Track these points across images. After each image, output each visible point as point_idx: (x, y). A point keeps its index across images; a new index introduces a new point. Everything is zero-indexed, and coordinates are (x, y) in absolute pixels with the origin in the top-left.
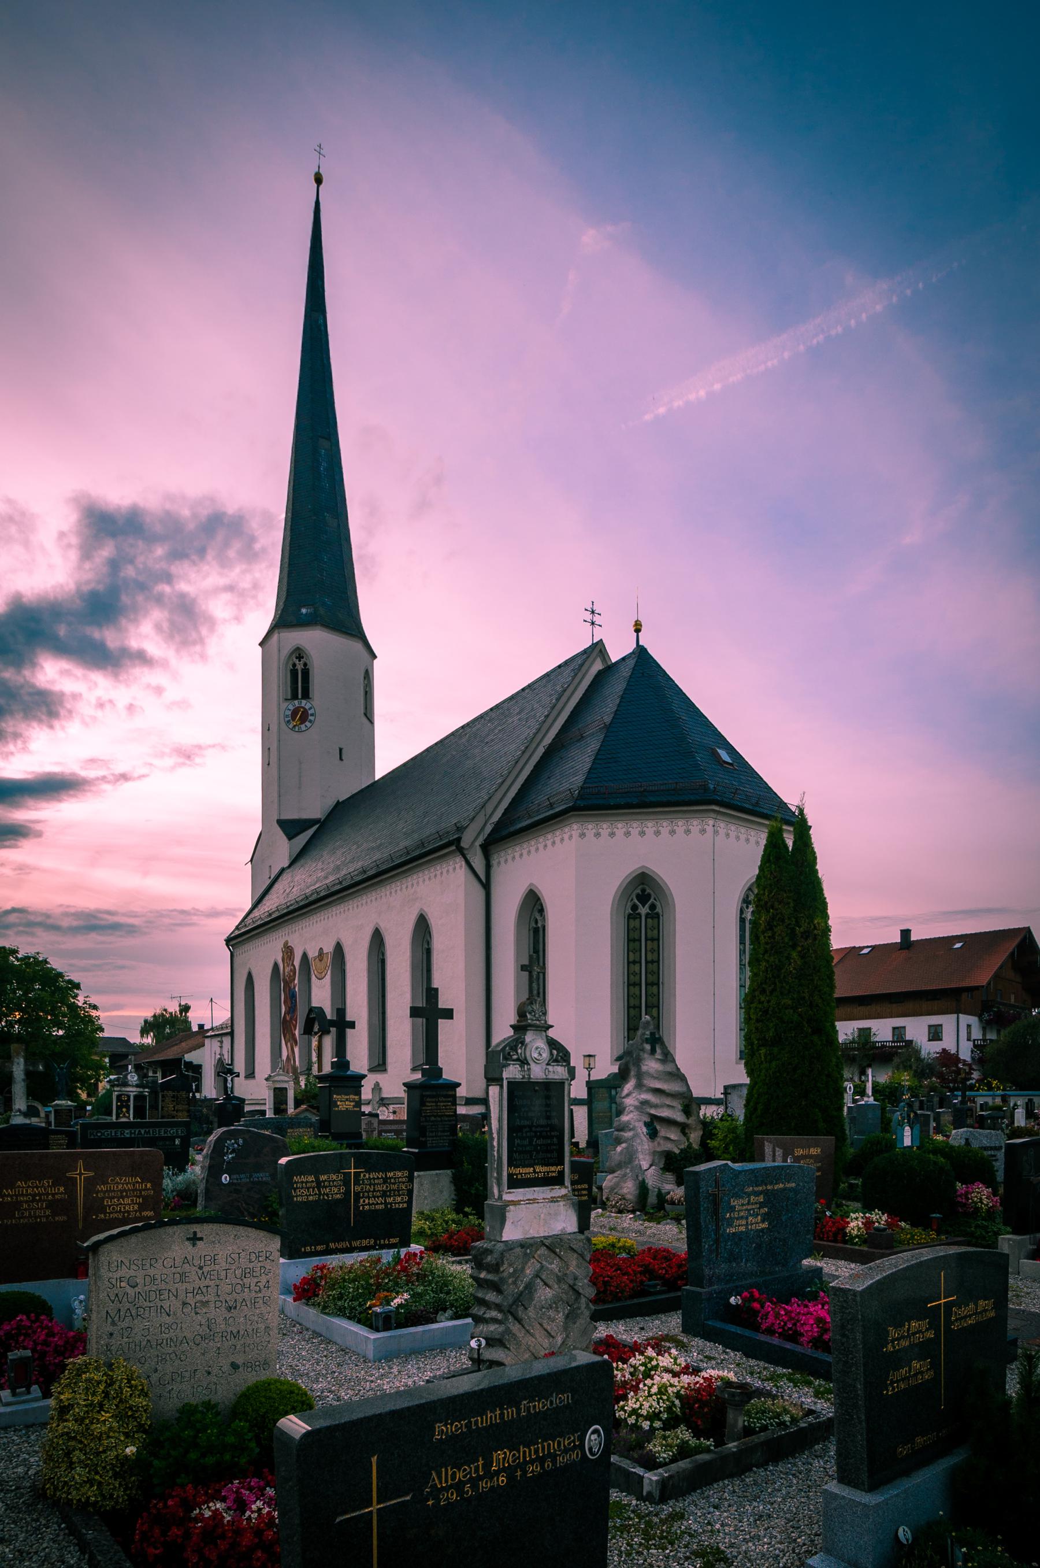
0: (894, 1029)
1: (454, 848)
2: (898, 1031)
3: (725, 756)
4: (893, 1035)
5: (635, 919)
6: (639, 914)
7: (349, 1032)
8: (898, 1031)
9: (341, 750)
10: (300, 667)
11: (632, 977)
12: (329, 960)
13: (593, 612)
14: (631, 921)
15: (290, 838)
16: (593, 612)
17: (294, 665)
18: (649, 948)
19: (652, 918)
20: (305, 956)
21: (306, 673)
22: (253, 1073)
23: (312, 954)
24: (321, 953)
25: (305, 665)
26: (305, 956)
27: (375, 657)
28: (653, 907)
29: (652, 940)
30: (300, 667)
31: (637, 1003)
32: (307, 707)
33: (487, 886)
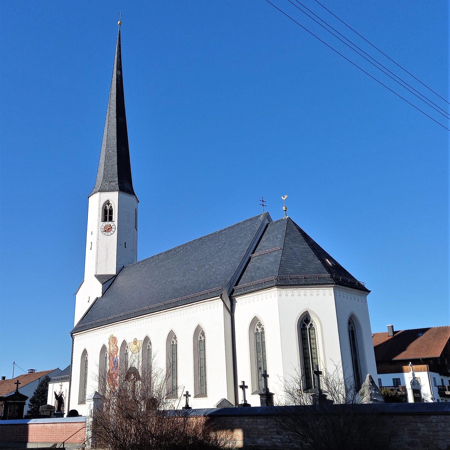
13: (263, 201)
16: (263, 201)
17: (106, 207)
21: (111, 211)
23: (129, 341)
24: (135, 342)
25: (111, 207)
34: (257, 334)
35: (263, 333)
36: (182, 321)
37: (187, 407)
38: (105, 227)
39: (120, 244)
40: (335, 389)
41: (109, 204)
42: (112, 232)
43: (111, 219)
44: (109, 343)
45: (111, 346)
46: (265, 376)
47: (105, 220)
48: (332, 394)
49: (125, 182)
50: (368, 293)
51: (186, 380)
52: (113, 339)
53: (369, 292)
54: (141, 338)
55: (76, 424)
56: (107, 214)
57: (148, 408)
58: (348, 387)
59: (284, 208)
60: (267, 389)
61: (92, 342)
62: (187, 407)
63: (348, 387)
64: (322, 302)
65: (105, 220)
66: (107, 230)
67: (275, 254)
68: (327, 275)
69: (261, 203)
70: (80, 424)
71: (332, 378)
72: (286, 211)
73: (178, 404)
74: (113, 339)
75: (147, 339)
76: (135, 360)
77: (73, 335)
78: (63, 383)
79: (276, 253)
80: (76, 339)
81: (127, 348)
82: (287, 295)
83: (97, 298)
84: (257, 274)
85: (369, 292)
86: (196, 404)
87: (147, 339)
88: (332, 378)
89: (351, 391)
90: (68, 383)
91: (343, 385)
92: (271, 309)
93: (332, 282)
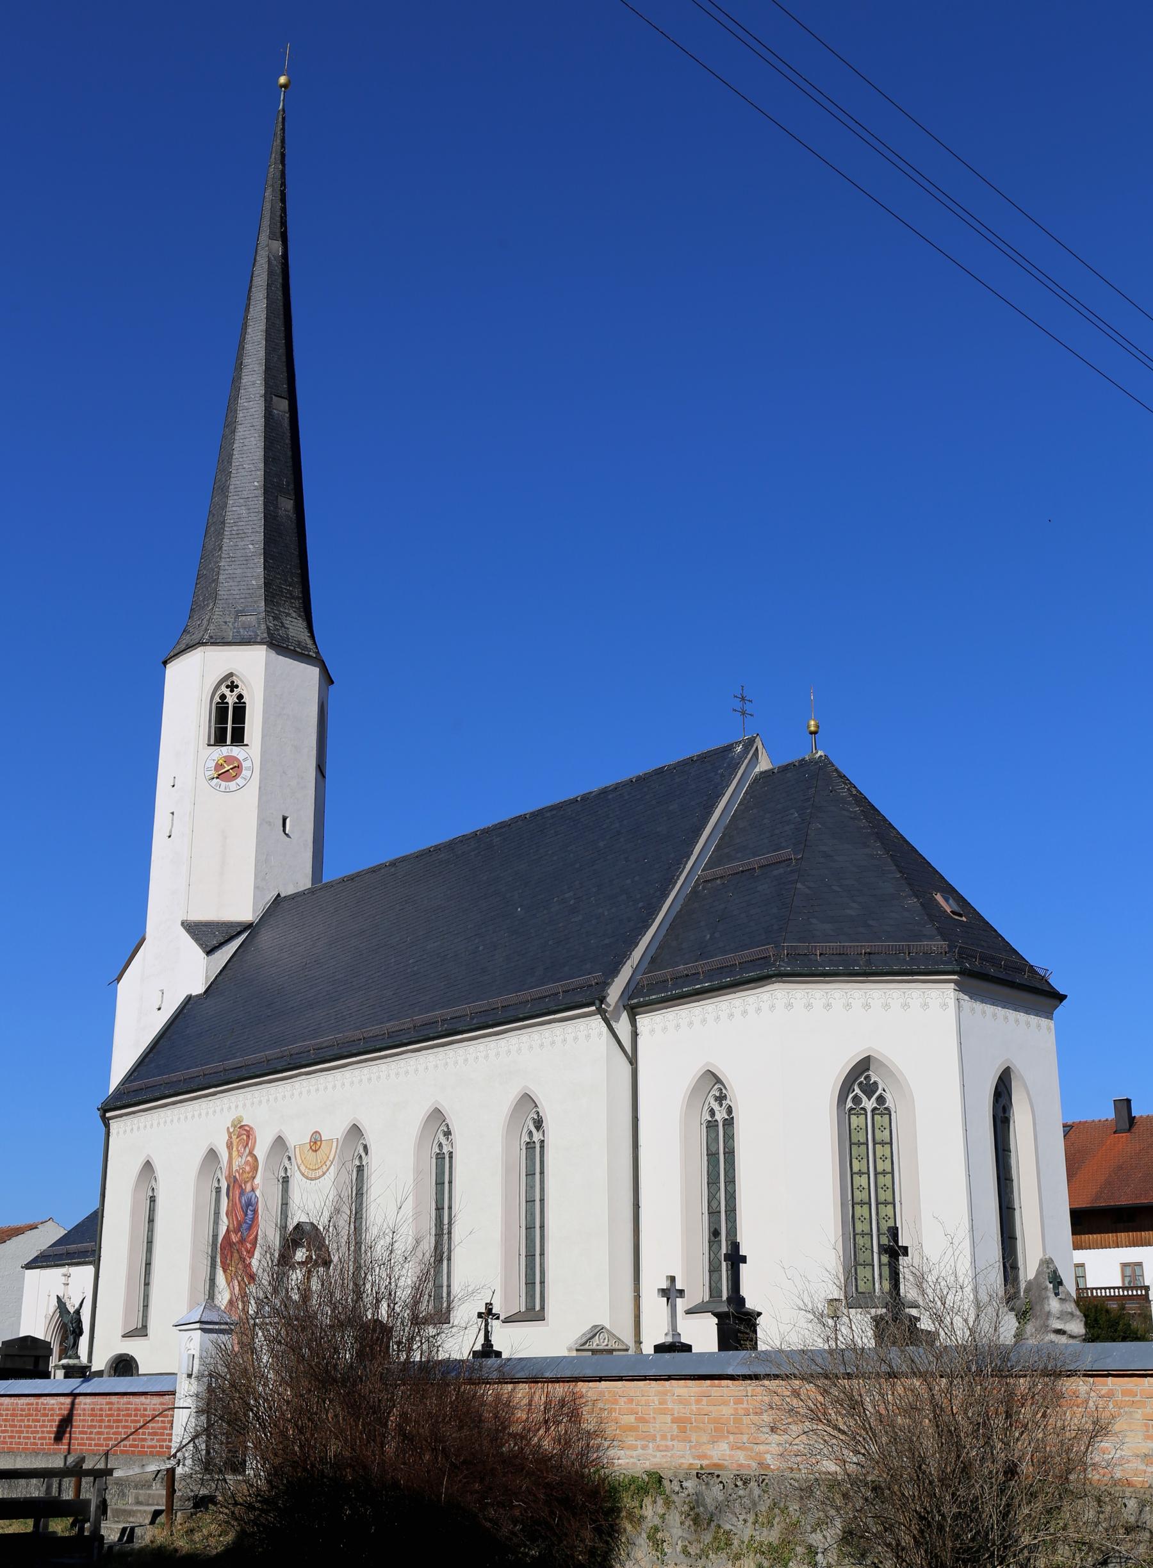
0: (1124, 1265)
1: (593, 1008)
2: (1132, 1270)
3: (947, 906)
4: (1124, 1276)
5: (858, 1115)
6: (864, 1109)
7: (903, 1261)
8: (1132, 1270)
9: (284, 819)
10: (231, 699)
11: (857, 1193)
12: (330, 1152)
13: (743, 699)
14: (853, 1117)
15: (209, 952)
16: (743, 699)
17: (223, 697)
18: (879, 1155)
19: (882, 1114)
20: (280, 1142)
21: (240, 711)
22: (145, 1327)
23: (297, 1138)
24: (316, 1142)
25: (240, 697)
26: (280, 1142)
27: (332, 683)
28: (881, 1100)
29: (883, 1143)
30: (231, 699)
31: (867, 1229)
32: (241, 758)
33: (633, 1060)
34: (711, 1126)
35: (729, 1123)
36: (475, 1078)
37: (488, 1351)
38: (218, 766)
39: (269, 823)
40: (944, 1304)
41: (232, 687)
42: (240, 781)
43: (238, 738)
44: (230, 1146)
45: (235, 1154)
46: (736, 1259)
47: (220, 739)
48: (938, 1318)
49: (288, 615)
50: (1056, 1002)
51: (480, 1270)
52: (243, 1134)
53: (1062, 998)
54: (334, 1130)
55: (142, 1399)
56: (228, 722)
57: (360, 1355)
58: (984, 1298)
59: (812, 723)
60: (737, 1299)
61: (176, 1141)
62: (488, 1351)
63: (984, 1298)
64: (919, 1028)
65: (220, 739)
66: (228, 772)
67: (776, 873)
68: (938, 945)
69: (738, 704)
70: (156, 1400)
71: (935, 1273)
72: (815, 733)
73: (458, 1343)
74: (243, 1134)
75: (356, 1131)
76: (313, 1200)
77: (108, 1115)
78: (74, 1270)
79: (781, 871)
80: (114, 1125)
81: (286, 1162)
82: (886, 1006)
83: (189, 998)
84: (717, 935)
85: (1062, 998)
86: (514, 1342)
87: (356, 1131)
88: (935, 1273)
89: (990, 1309)
90: (91, 1269)
91: (968, 1290)
92: (779, 1044)
93: (949, 968)
